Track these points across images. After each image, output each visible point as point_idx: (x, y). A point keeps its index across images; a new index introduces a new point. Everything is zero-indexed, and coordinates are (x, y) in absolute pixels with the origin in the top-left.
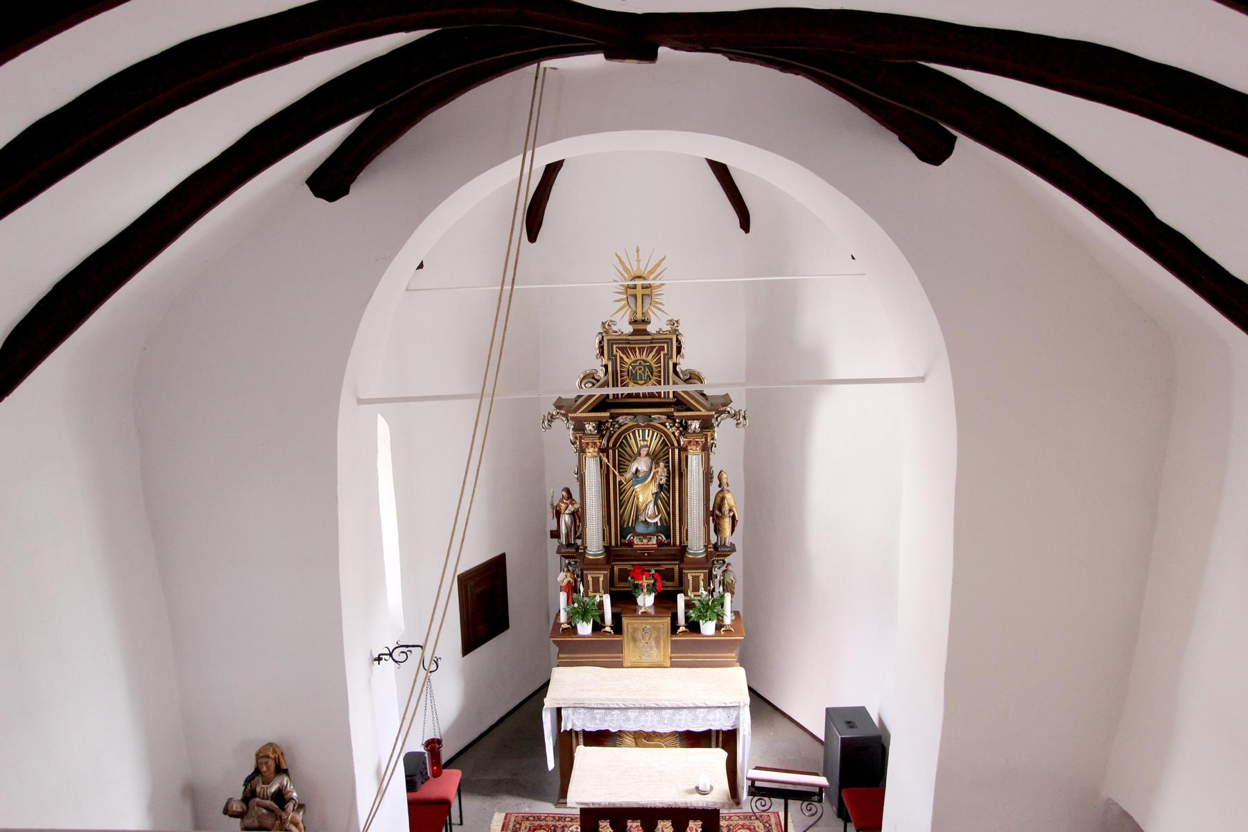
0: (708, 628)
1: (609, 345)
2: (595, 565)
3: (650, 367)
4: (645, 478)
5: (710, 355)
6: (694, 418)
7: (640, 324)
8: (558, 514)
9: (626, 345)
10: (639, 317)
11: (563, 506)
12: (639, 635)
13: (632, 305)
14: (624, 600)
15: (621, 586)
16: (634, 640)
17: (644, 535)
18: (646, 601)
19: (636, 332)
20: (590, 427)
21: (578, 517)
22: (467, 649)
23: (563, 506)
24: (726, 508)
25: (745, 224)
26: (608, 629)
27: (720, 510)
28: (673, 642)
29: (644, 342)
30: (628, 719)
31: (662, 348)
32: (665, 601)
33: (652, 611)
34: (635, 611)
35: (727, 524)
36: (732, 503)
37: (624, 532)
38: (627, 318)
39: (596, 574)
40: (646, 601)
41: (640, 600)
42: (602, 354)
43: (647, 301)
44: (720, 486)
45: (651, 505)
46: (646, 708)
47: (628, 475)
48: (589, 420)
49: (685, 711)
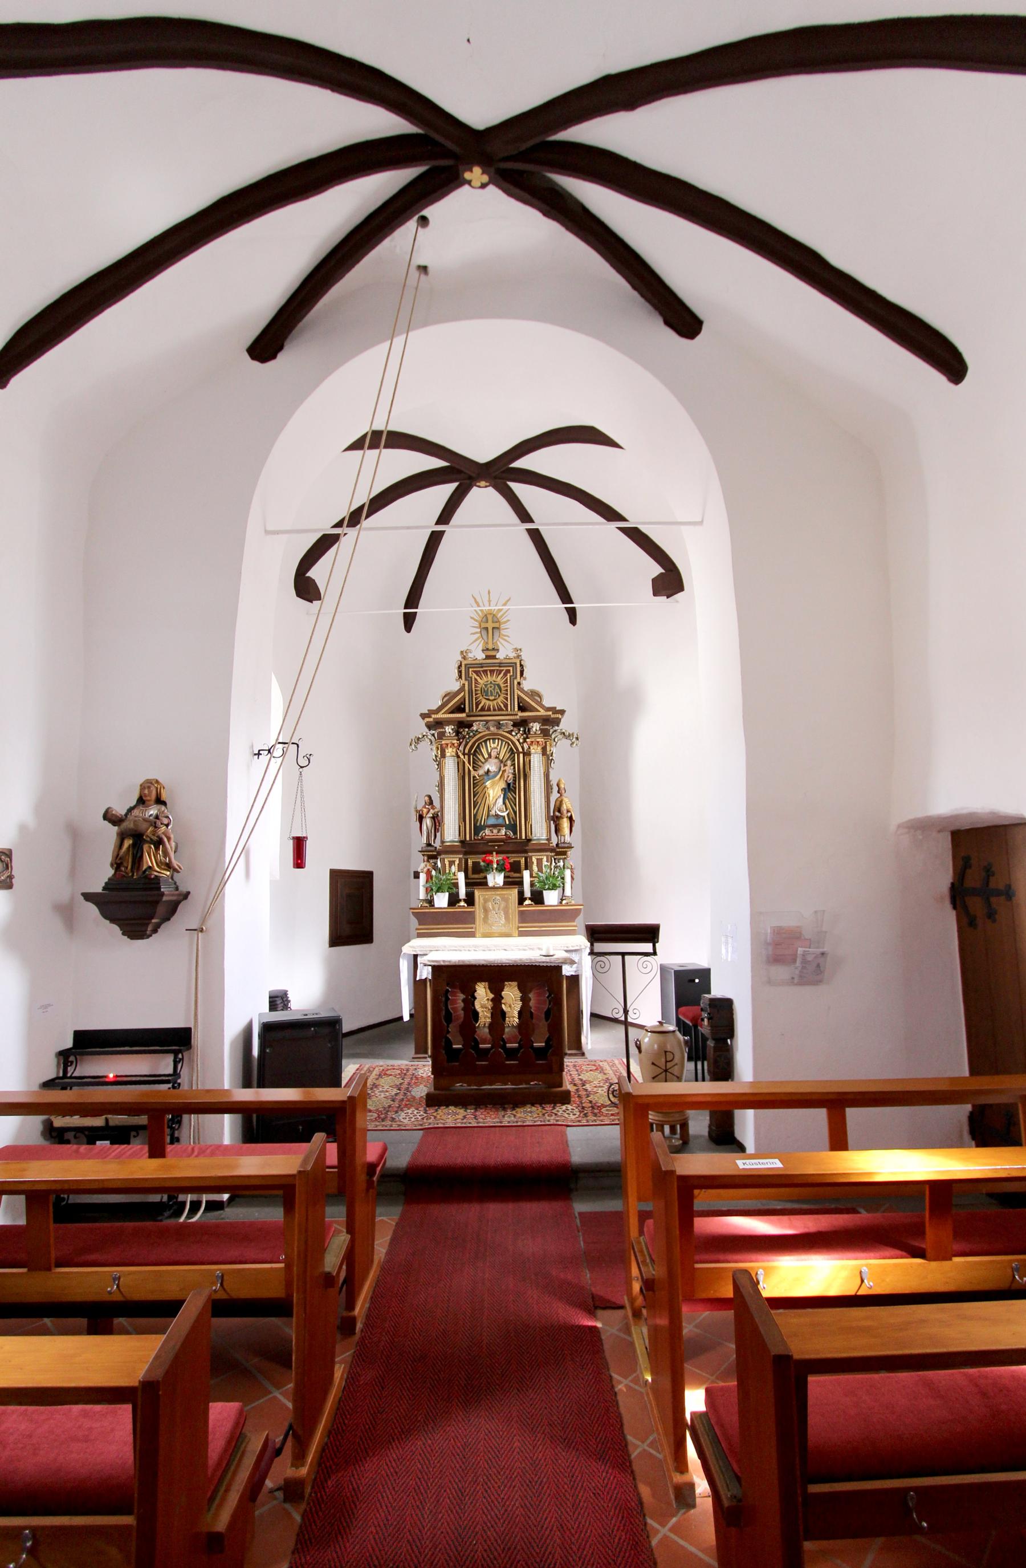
0: (551, 898)
1: (466, 669)
3: (499, 685)
5: (547, 681)
6: (535, 719)
7: (490, 653)
8: (421, 818)
9: (480, 669)
10: (490, 647)
11: (425, 810)
13: (485, 637)
14: (476, 881)
17: (494, 826)
18: (496, 879)
19: (488, 657)
20: (449, 729)
23: (425, 810)
24: (564, 808)
27: (559, 811)
28: (521, 913)
29: (493, 665)
31: (508, 671)
32: (513, 882)
35: (565, 824)
36: (569, 806)
37: (478, 829)
38: (481, 648)
40: (496, 879)
42: (460, 677)
43: (496, 633)
45: (501, 801)
47: (481, 772)
48: (448, 722)
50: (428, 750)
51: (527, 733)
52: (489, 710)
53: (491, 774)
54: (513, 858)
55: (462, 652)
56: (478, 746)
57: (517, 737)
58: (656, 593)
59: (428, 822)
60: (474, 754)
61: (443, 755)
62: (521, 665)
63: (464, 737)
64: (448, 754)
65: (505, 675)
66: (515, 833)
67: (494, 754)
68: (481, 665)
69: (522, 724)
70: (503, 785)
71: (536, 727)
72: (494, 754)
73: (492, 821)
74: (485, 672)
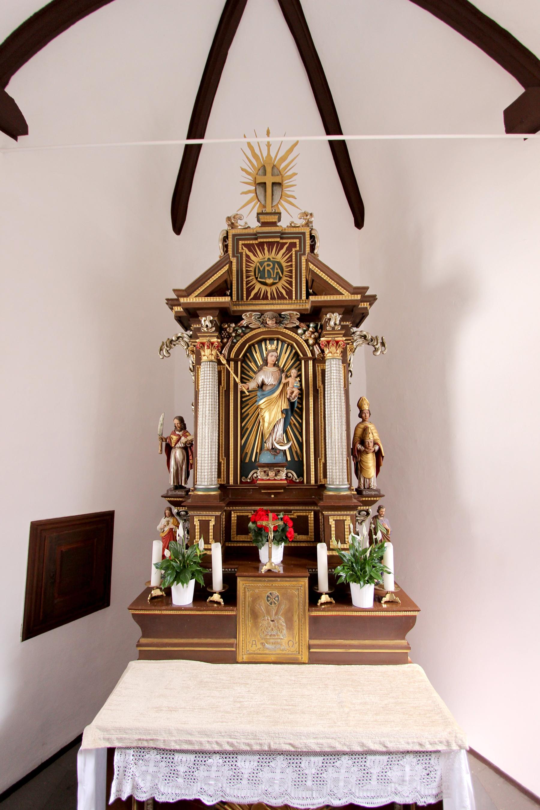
0: (363, 596)
2: (204, 504)
3: (279, 264)
4: (273, 391)
8: (169, 449)
9: (257, 241)
10: (269, 210)
11: (175, 438)
12: (262, 606)
13: (261, 198)
14: (243, 557)
15: (240, 540)
16: (255, 615)
17: (271, 466)
18: (272, 555)
20: (206, 321)
21: (189, 449)
22: (33, 627)
25: (359, 223)
26: (216, 597)
27: (363, 442)
28: (314, 620)
30: (237, 777)
31: (293, 245)
32: (300, 558)
33: (281, 570)
34: (257, 569)
35: (370, 460)
37: (246, 467)
39: (205, 515)
40: (272, 555)
41: (263, 553)
44: (360, 416)
46: (272, 753)
47: (252, 385)
48: (206, 309)
49: (345, 760)
50: (181, 355)
51: (320, 331)
52: (265, 297)
53: (267, 389)
54: (297, 512)
55: (229, 219)
56: (249, 350)
57: (305, 336)
58: (510, 129)
59: (177, 454)
60: (243, 361)
61: (198, 361)
62: (312, 238)
63: (229, 336)
64: (204, 358)
65: (289, 250)
66: (300, 474)
67: (271, 359)
68: (256, 236)
69: (313, 316)
70: (286, 406)
71: (334, 318)
72: (271, 359)
73: (266, 458)
74: (261, 245)
